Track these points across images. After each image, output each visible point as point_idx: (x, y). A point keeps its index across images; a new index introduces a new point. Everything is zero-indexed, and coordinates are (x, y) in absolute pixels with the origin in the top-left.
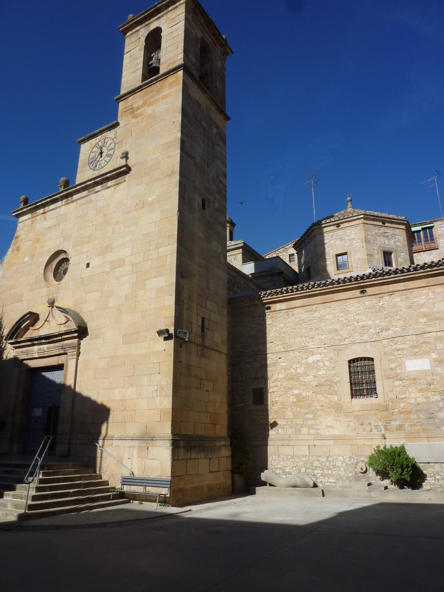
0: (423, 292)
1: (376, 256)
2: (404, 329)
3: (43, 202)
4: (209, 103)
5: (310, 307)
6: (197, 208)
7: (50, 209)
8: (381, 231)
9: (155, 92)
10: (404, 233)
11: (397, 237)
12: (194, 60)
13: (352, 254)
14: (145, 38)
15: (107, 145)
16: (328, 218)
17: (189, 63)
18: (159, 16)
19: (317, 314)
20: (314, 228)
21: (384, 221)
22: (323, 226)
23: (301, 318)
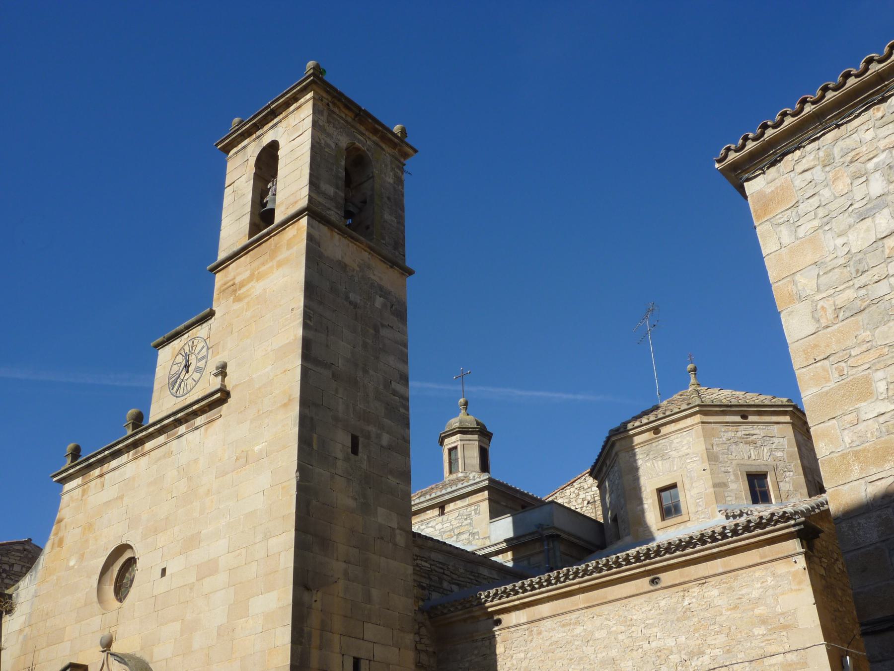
0: (757, 575)
1: (733, 486)
2: (728, 651)
3: (99, 457)
4: (366, 255)
5: (568, 617)
6: (340, 455)
7: (110, 468)
8: (739, 434)
9: (266, 257)
10: (789, 431)
11: (776, 440)
12: (331, 191)
13: (687, 486)
14: (255, 159)
15: (197, 352)
16: (646, 413)
17: (321, 199)
18: (276, 121)
19: (579, 630)
20: (613, 439)
21: (744, 412)
22: (631, 432)
23: (554, 639)
